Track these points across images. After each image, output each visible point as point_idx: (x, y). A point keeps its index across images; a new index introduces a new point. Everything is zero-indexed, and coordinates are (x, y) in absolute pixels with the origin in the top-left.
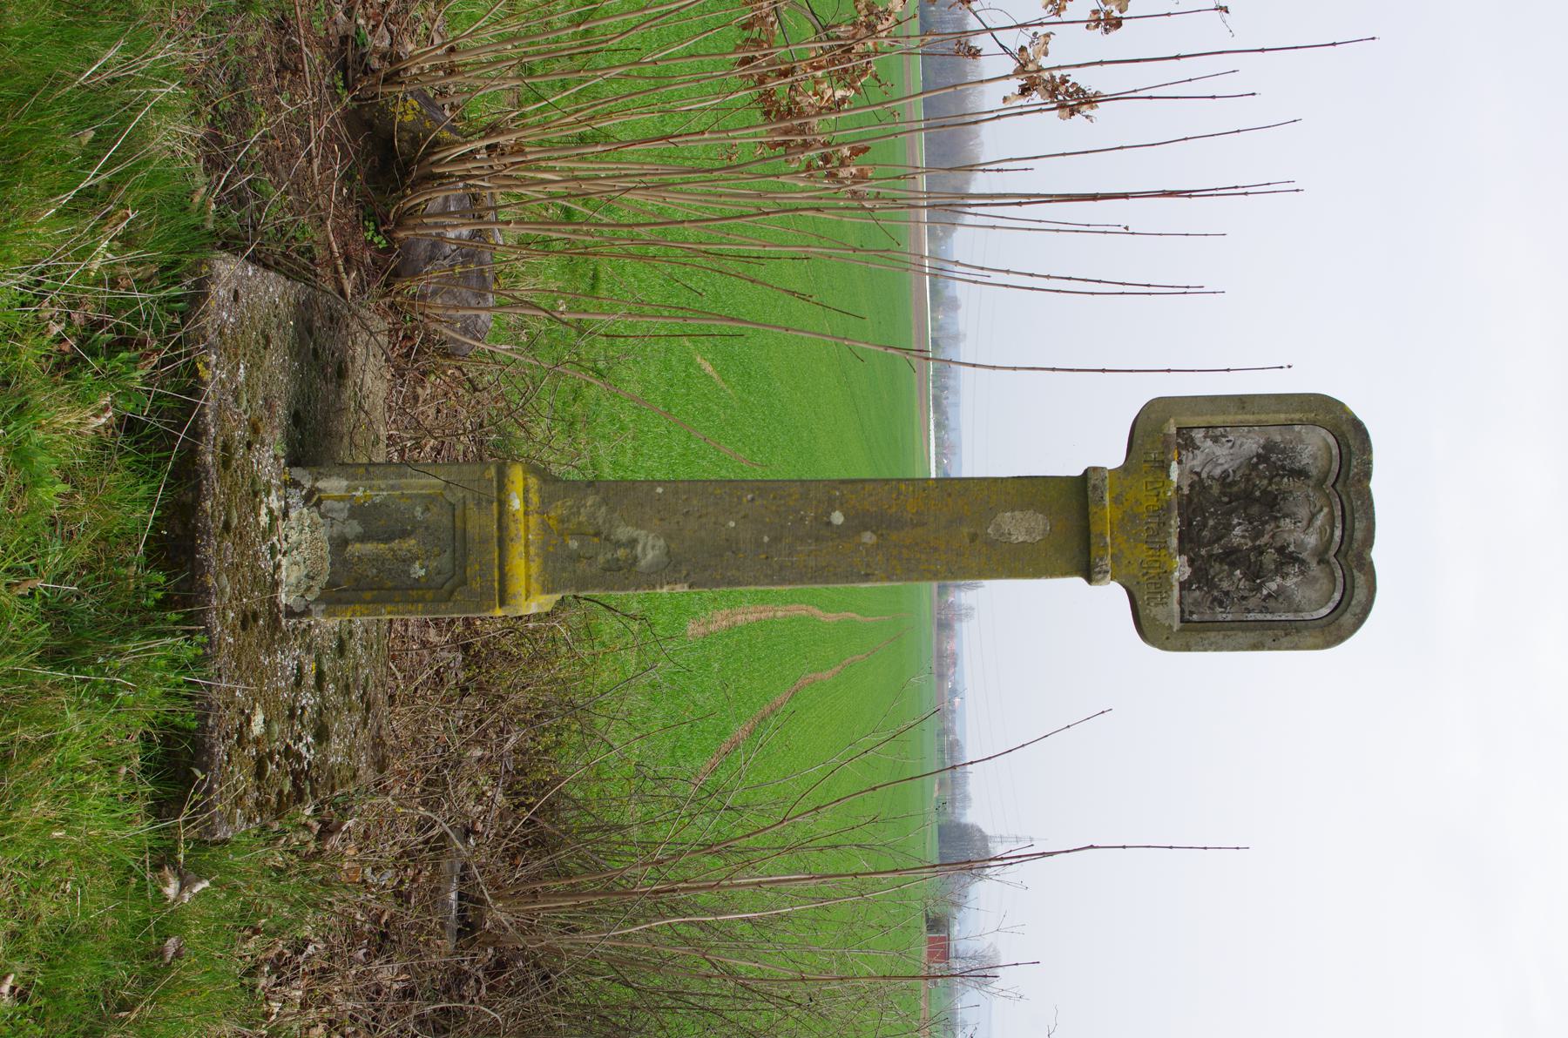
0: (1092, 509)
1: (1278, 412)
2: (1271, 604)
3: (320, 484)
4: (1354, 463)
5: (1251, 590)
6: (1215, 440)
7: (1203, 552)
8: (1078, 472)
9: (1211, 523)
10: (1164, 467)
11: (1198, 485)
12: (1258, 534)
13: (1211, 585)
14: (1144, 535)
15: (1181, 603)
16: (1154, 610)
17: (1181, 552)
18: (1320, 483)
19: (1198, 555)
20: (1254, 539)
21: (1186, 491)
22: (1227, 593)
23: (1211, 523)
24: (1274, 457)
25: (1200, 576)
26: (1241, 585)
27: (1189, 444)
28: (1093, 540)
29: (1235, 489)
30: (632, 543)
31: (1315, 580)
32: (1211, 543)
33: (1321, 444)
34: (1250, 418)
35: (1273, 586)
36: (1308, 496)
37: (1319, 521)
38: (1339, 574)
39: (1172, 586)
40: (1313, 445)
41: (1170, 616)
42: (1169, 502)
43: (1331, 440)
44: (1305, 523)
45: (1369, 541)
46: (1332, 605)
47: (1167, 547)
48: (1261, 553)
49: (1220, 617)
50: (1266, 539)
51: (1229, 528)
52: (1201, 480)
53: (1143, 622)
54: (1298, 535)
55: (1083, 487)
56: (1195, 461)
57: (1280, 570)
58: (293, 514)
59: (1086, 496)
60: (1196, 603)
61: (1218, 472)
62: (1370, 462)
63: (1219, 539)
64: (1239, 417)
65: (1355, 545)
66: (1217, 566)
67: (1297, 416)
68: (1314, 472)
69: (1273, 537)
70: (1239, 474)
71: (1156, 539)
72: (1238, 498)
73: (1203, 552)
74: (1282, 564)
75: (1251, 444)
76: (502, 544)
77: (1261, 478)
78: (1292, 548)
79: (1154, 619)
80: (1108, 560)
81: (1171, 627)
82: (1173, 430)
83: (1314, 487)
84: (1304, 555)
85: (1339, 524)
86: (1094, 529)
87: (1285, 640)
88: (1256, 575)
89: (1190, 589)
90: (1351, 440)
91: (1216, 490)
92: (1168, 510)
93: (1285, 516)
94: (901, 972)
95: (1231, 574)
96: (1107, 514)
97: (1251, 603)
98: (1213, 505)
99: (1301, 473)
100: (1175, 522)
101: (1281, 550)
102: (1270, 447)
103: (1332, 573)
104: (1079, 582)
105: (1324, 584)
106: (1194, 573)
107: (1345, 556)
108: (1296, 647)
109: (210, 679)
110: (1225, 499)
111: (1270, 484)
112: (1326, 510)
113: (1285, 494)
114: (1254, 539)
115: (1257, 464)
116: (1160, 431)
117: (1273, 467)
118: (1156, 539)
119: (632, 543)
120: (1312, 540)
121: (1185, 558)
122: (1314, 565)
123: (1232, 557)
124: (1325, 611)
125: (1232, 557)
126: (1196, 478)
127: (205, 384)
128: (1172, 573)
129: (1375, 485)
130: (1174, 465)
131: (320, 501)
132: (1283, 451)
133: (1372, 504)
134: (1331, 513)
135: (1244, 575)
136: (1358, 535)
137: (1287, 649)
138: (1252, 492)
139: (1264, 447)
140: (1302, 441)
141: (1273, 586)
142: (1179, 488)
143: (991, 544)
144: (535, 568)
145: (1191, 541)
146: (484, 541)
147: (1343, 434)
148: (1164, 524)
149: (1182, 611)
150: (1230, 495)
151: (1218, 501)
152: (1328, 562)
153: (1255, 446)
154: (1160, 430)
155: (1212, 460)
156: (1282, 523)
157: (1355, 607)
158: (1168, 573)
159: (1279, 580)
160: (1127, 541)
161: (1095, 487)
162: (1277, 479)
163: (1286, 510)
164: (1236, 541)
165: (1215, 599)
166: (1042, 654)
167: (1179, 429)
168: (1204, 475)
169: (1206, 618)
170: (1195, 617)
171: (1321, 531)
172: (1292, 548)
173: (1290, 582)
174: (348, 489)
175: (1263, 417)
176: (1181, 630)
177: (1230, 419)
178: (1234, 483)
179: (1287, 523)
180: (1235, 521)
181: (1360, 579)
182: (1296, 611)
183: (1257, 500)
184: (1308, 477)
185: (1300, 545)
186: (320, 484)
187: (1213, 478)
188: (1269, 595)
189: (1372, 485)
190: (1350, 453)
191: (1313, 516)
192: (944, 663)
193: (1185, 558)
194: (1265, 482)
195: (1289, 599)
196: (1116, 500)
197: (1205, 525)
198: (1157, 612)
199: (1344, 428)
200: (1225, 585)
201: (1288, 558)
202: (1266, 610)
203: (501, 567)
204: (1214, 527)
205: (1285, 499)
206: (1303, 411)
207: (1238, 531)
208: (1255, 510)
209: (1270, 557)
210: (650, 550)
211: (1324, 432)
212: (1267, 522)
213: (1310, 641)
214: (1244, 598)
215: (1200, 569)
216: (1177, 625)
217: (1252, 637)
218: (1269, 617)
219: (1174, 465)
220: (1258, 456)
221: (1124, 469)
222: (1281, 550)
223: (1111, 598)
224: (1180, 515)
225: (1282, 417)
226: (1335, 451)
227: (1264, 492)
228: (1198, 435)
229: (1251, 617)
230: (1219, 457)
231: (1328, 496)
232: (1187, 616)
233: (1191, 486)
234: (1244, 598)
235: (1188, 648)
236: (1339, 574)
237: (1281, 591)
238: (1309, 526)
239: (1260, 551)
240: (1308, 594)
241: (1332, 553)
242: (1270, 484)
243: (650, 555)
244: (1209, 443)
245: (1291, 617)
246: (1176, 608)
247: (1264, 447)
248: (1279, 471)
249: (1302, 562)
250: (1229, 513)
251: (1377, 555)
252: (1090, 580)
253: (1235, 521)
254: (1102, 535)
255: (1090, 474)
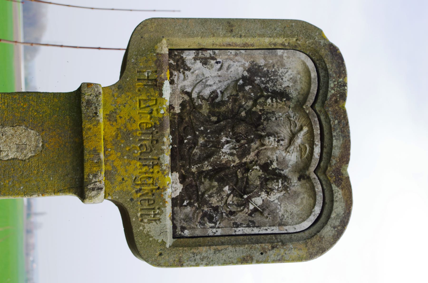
0: (86, 125)
1: (263, 36)
2: (257, 218)
4: (332, 85)
5: (239, 205)
6: (205, 62)
7: (194, 169)
8: (73, 88)
9: (201, 141)
10: (157, 86)
11: (189, 104)
12: (244, 152)
13: (202, 201)
14: (137, 153)
15: (173, 219)
16: (147, 226)
17: (173, 169)
18: (300, 105)
19: (188, 171)
20: (241, 157)
21: (177, 110)
22: (216, 209)
23: (201, 141)
24: (258, 80)
25: (191, 193)
26: (230, 201)
27: (180, 66)
28: (87, 157)
29: (223, 109)
31: (296, 194)
32: (201, 160)
33: (300, 68)
34: (238, 41)
35: (258, 201)
36: (288, 117)
38: (319, 188)
39: (164, 202)
40: (293, 69)
41: (163, 232)
42: (161, 120)
43: (310, 64)
44: (286, 141)
45: (345, 158)
46: (313, 218)
47: (160, 165)
48: (247, 170)
49: (210, 232)
50: (251, 156)
51: (218, 146)
52: (192, 100)
53: (138, 240)
54: (280, 153)
55: (76, 104)
56: (186, 82)
57: (265, 186)
59: (80, 112)
60: (188, 219)
61: (207, 92)
62: (345, 85)
63: (209, 156)
64: (228, 40)
65: (333, 162)
66: (207, 183)
67: (280, 40)
68: (294, 94)
69: (257, 155)
70: (227, 94)
71: (149, 157)
72: (225, 118)
73: (194, 169)
74: (267, 180)
75: (238, 67)
77: (247, 99)
78: (275, 165)
79: (148, 235)
80: (102, 177)
81: (163, 243)
82: (166, 51)
83: (295, 109)
84: (286, 172)
85: (318, 142)
86: (88, 145)
87: (272, 253)
88: (243, 191)
89: (181, 205)
90: (328, 63)
91: (205, 110)
92: (161, 127)
93: (269, 135)
94: (263, 51)
95: (220, 190)
96: (100, 131)
97: (240, 217)
98: (203, 124)
99: (283, 95)
100: (167, 139)
101: (265, 167)
102: (254, 70)
103: (313, 188)
104: (72, 199)
105: (304, 198)
106: (185, 189)
107: (324, 172)
108: (281, 260)
110: (214, 119)
111: (255, 105)
112: (305, 129)
113: (268, 115)
114: (241, 157)
115: (243, 86)
116: (154, 50)
117: (256, 88)
118: (149, 157)
120: (293, 158)
121: (176, 175)
122: (295, 180)
123: (221, 174)
124: (306, 224)
125: (221, 174)
126: (186, 98)
128: (164, 189)
130: (167, 83)
132: (266, 75)
134: (311, 132)
135: (233, 190)
136: (336, 152)
137: (274, 261)
138: (238, 113)
139: (249, 71)
140: (283, 65)
141: (258, 201)
142: (171, 107)
145: (182, 158)
147: (321, 59)
148: (157, 142)
149: (174, 227)
150: (218, 115)
151: (207, 121)
152: (309, 178)
153: (241, 69)
154: (152, 52)
155: (201, 81)
156: (267, 141)
157: (334, 221)
158: (161, 189)
159: (264, 195)
160: (121, 158)
161: (89, 103)
162: (261, 100)
163: (269, 130)
164: (225, 158)
165: (205, 215)
167: (170, 50)
168: (194, 95)
169: (198, 232)
170: (187, 233)
171: (301, 149)
172: (275, 165)
173: (274, 197)
175: (249, 40)
176: (174, 246)
177: (219, 41)
178: (222, 103)
179: (271, 141)
180: (224, 139)
181: (338, 193)
182: (280, 225)
183: (243, 120)
184: (289, 99)
185: (282, 162)
187: (203, 98)
188: (255, 210)
190: (327, 76)
191: (293, 136)
192: (29, 248)
193: (176, 175)
194: (250, 103)
195: (273, 213)
196: (111, 117)
197: (195, 143)
198: (151, 228)
199: (323, 52)
200: (214, 201)
201: (272, 175)
202: (252, 224)
204: (204, 145)
205: (268, 119)
206: (285, 35)
207: (226, 149)
208: (241, 129)
209: (256, 173)
211: (303, 56)
212: (252, 141)
213: (295, 253)
214: (232, 213)
215: (191, 185)
216: (169, 241)
217: (242, 251)
218: (256, 231)
219: (167, 83)
220: (244, 78)
221: (119, 87)
222: (265, 167)
223: (102, 216)
224: (172, 133)
225: (266, 41)
226: (314, 74)
227: (249, 112)
228: (189, 56)
229: (240, 231)
230: (208, 79)
231: (307, 116)
232: (179, 232)
233: (183, 105)
234: (232, 213)
235: (180, 264)
236: (319, 188)
237: (266, 205)
238: (290, 144)
239: (246, 168)
240: (290, 207)
241: (312, 169)
242: (255, 105)
244: (198, 64)
245: (276, 230)
246: (169, 224)
247: (249, 71)
248: (261, 93)
249: (285, 178)
250: (218, 132)
251: (354, 170)
252: (83, 197)
253: (224, 139)
254: (96, 152)
255: (84, 90)
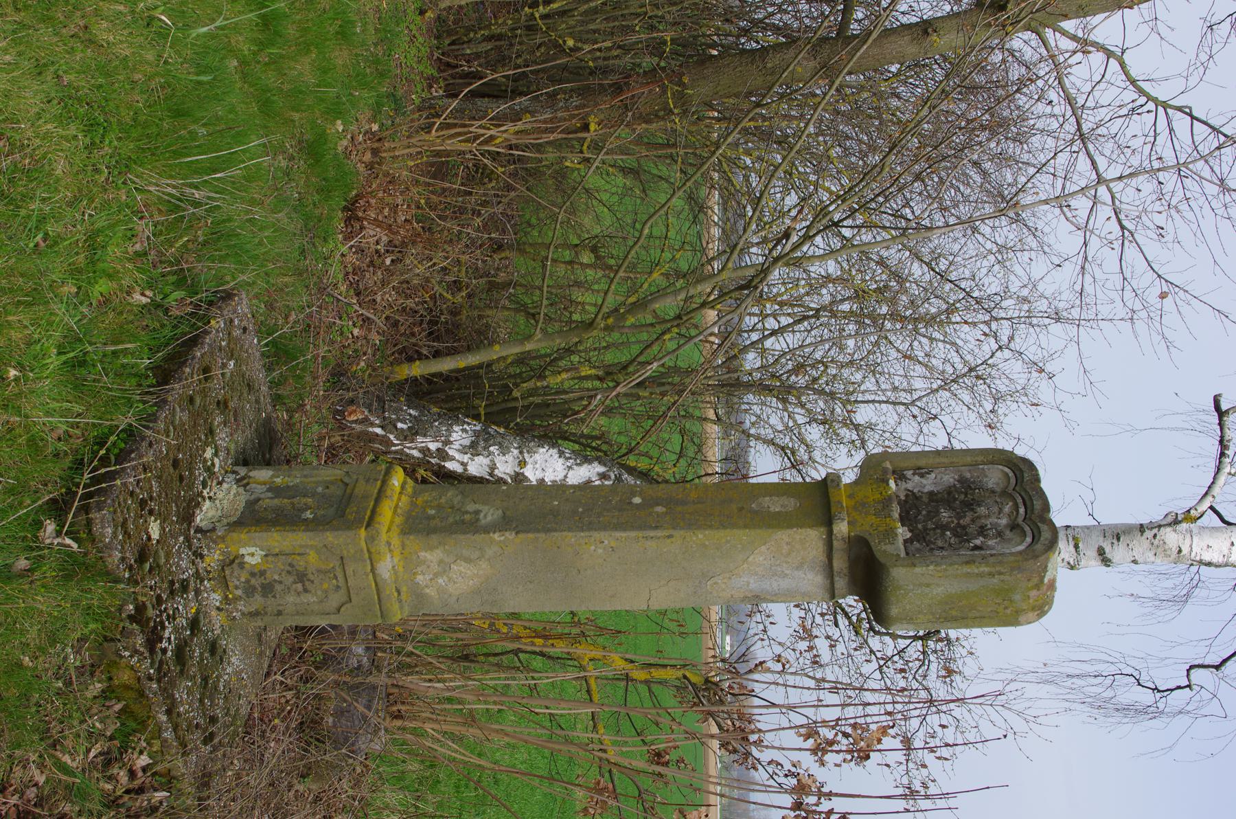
3: (251, 474)
6: (922, 476)
20: (959, 519)
30: (477, 512)
37: (1007, 509)
58: (225, 486)
75: (949, 478)
76: (378, 500)
109: (158, 433)
119: (477, 512)
127: (353, 23)
129: (1044, 485)
131: (248, 484)
133: (1044, 493)
143: (756, 512)
144: (398, 520)
146: (366, 497)
166: (789, 635)
174: (273, 476)
186: (251, 474)
189: (1043, 485)
203: (374, 512)
210: (490, 514)
216: (903, 554)
226: (1011, 474)
228: (909, 473)
243: (489, 518)
244: (917, 477)
254: (840, 502)
